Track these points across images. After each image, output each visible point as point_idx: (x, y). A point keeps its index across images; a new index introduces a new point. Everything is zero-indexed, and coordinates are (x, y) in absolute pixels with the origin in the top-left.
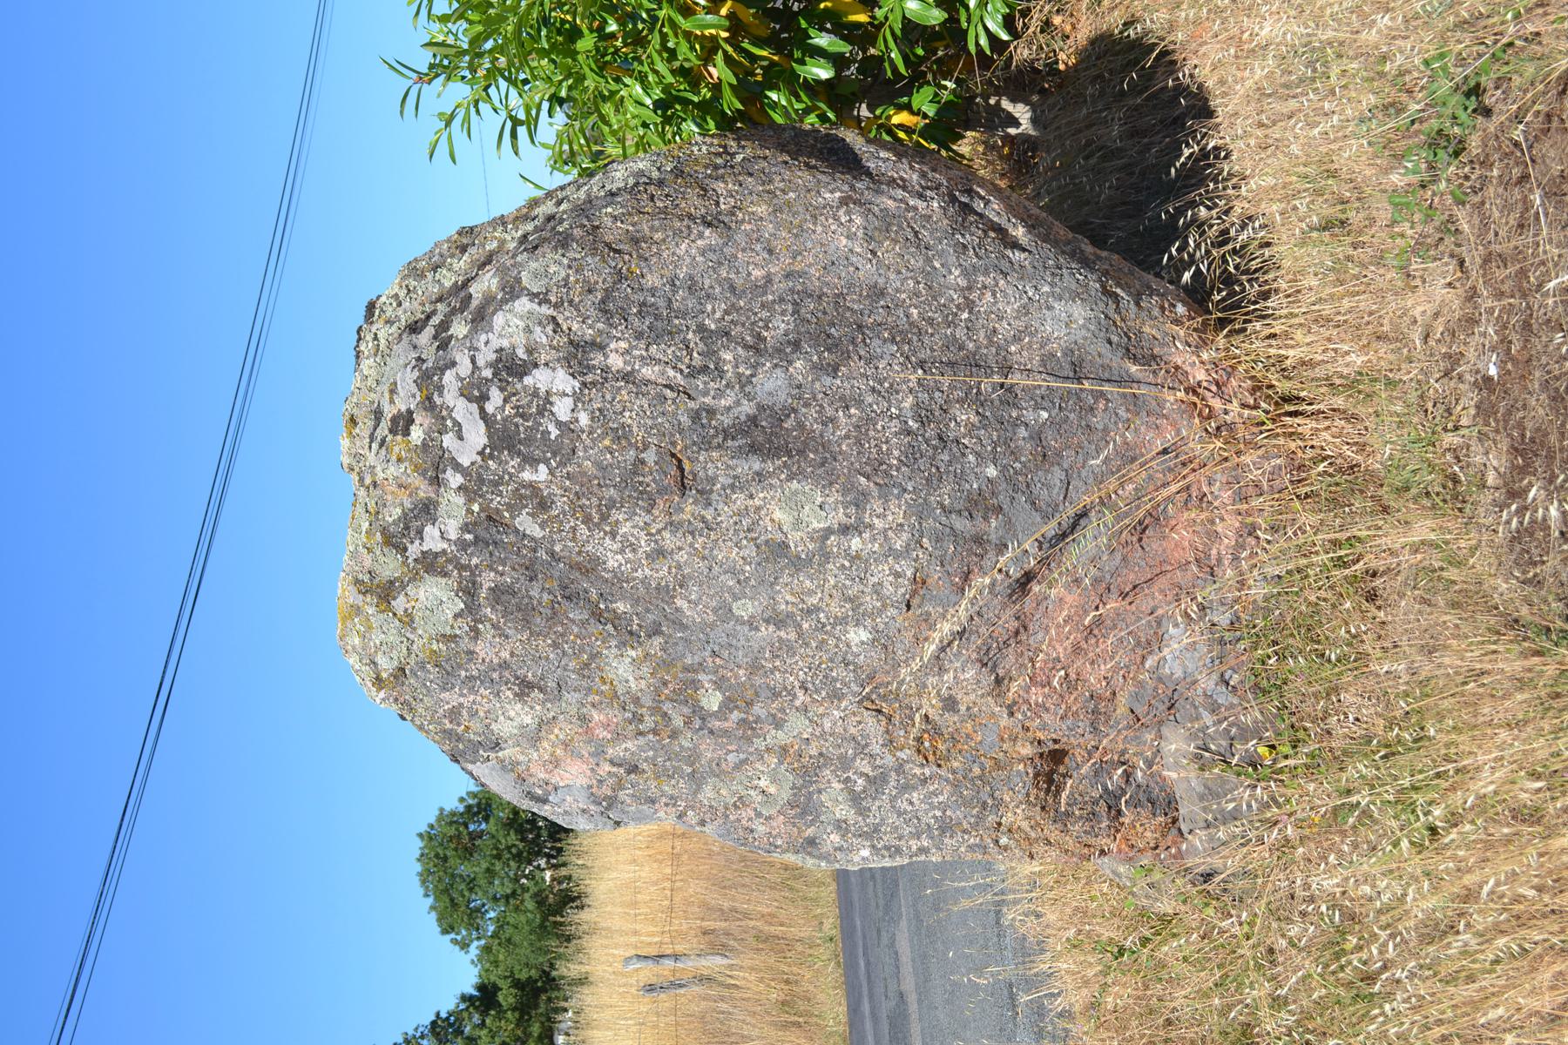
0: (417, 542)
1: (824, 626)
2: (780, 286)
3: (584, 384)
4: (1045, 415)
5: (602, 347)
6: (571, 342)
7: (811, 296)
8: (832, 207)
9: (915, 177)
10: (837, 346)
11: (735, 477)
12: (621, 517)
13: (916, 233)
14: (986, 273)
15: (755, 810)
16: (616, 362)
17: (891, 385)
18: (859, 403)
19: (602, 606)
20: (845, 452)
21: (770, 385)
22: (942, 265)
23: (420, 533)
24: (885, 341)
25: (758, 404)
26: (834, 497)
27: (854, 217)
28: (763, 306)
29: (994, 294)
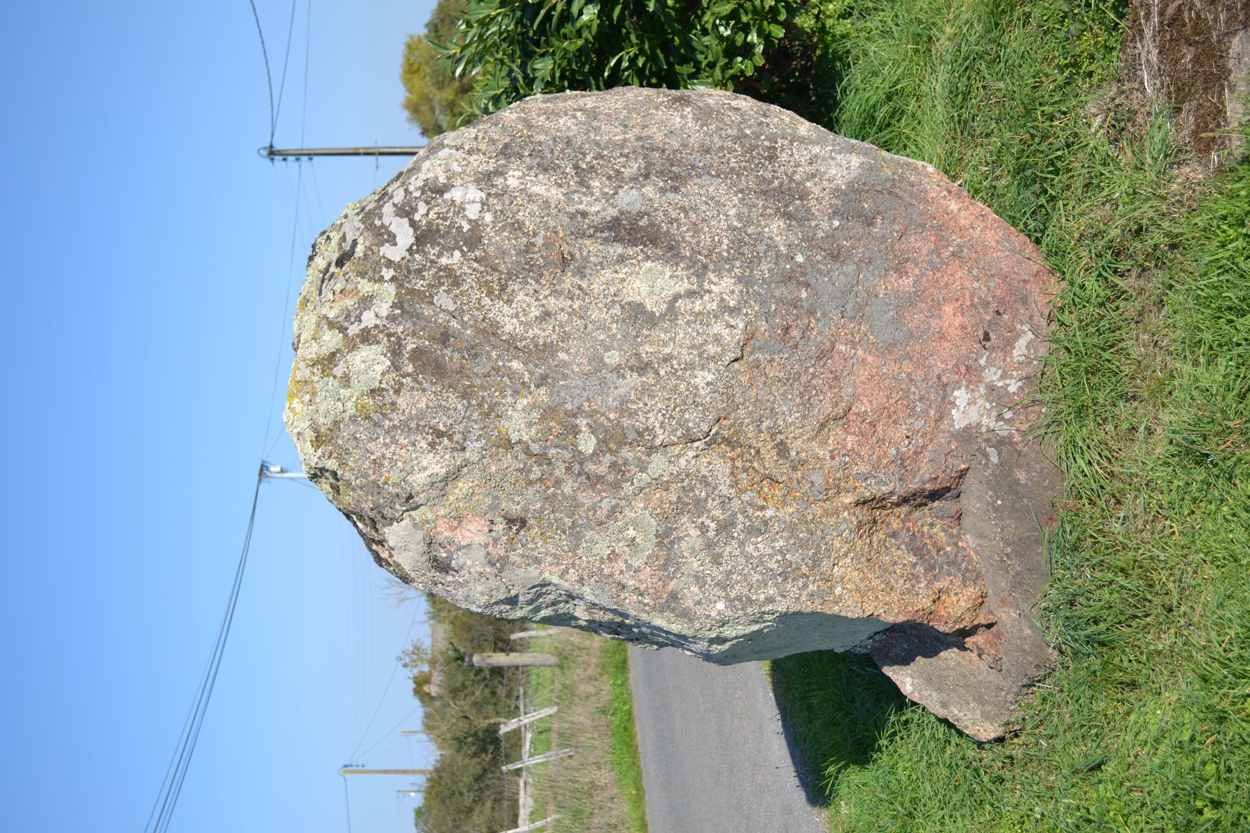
1: (676, 371)
3: (489, 195)
12: (516, 288)
15: (626, 561)
25: (620, 210)
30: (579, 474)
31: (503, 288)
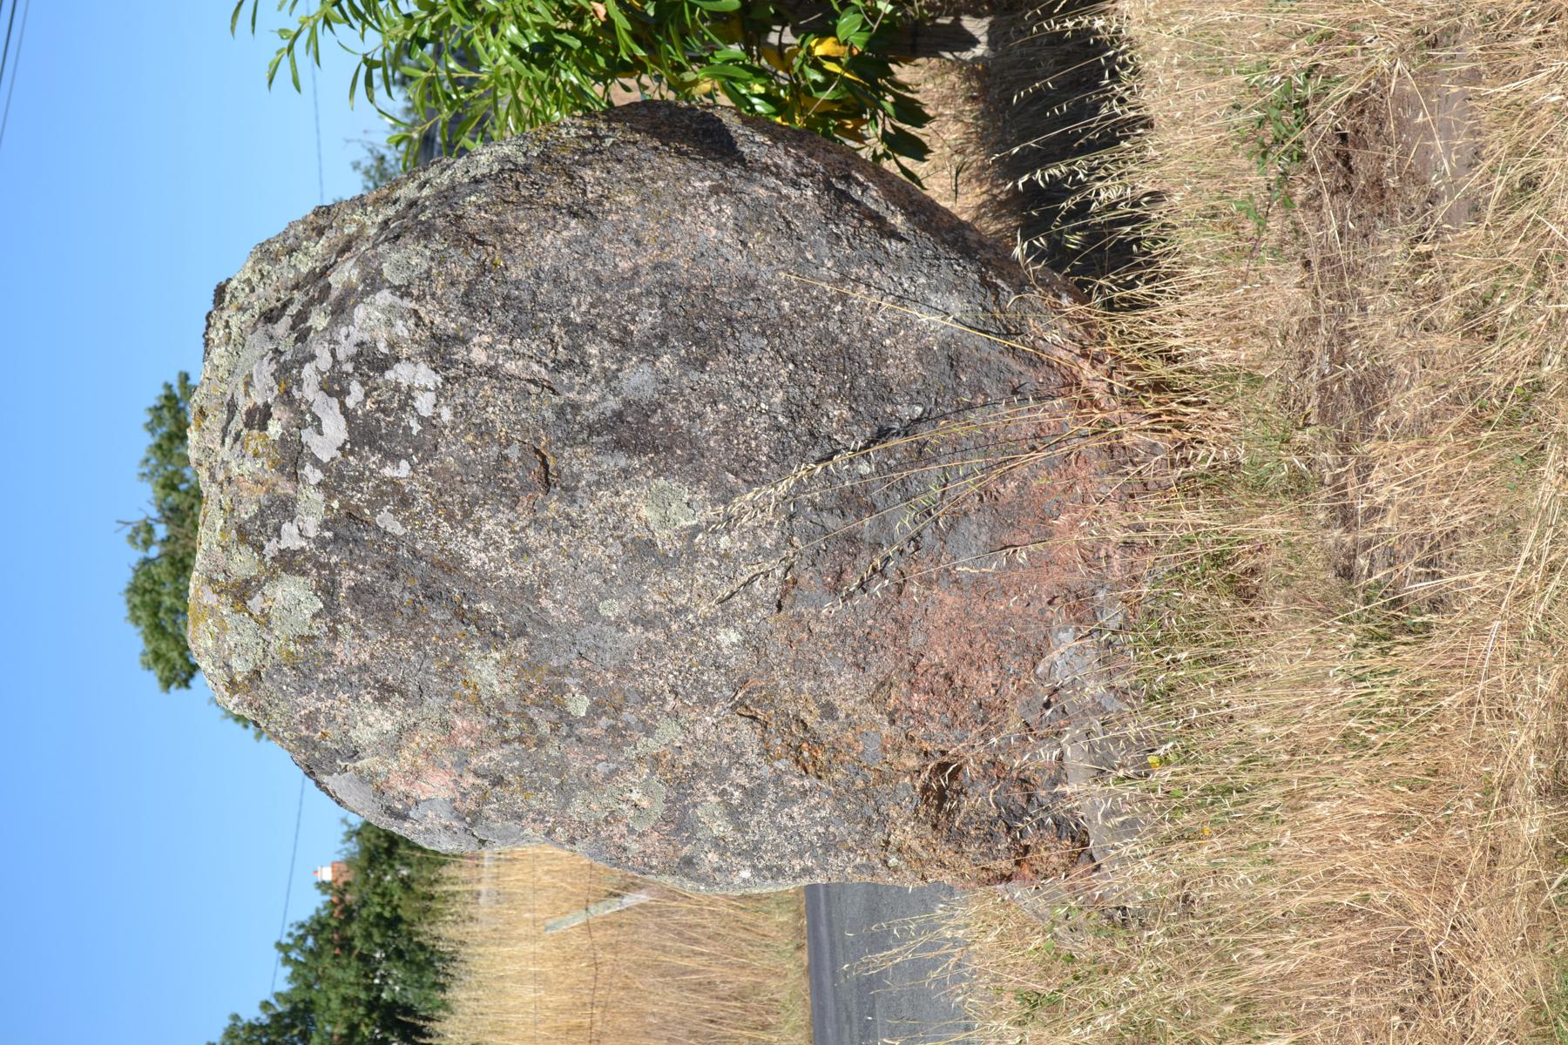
0: (275, 540)
2: (647, 279)
3: (447, 379)
5: (464, 342)
6: (433, 336)
7: (679, 288)
9: (790, 163)
11: (601, 474)
12: (484, 515)
13: (788, 223)
14: (860, 264)
16: (479, 356)
17: (761, 380)
18: (728, 398)
20: (713, 449)
21: (636, 380)
22: (815, 256)
23: (277, 530)
24: (755, 334)
25: (624, 400)
27: (724, 207)
28: (630, 299)
30: (568, 736)
31: (467, 515)
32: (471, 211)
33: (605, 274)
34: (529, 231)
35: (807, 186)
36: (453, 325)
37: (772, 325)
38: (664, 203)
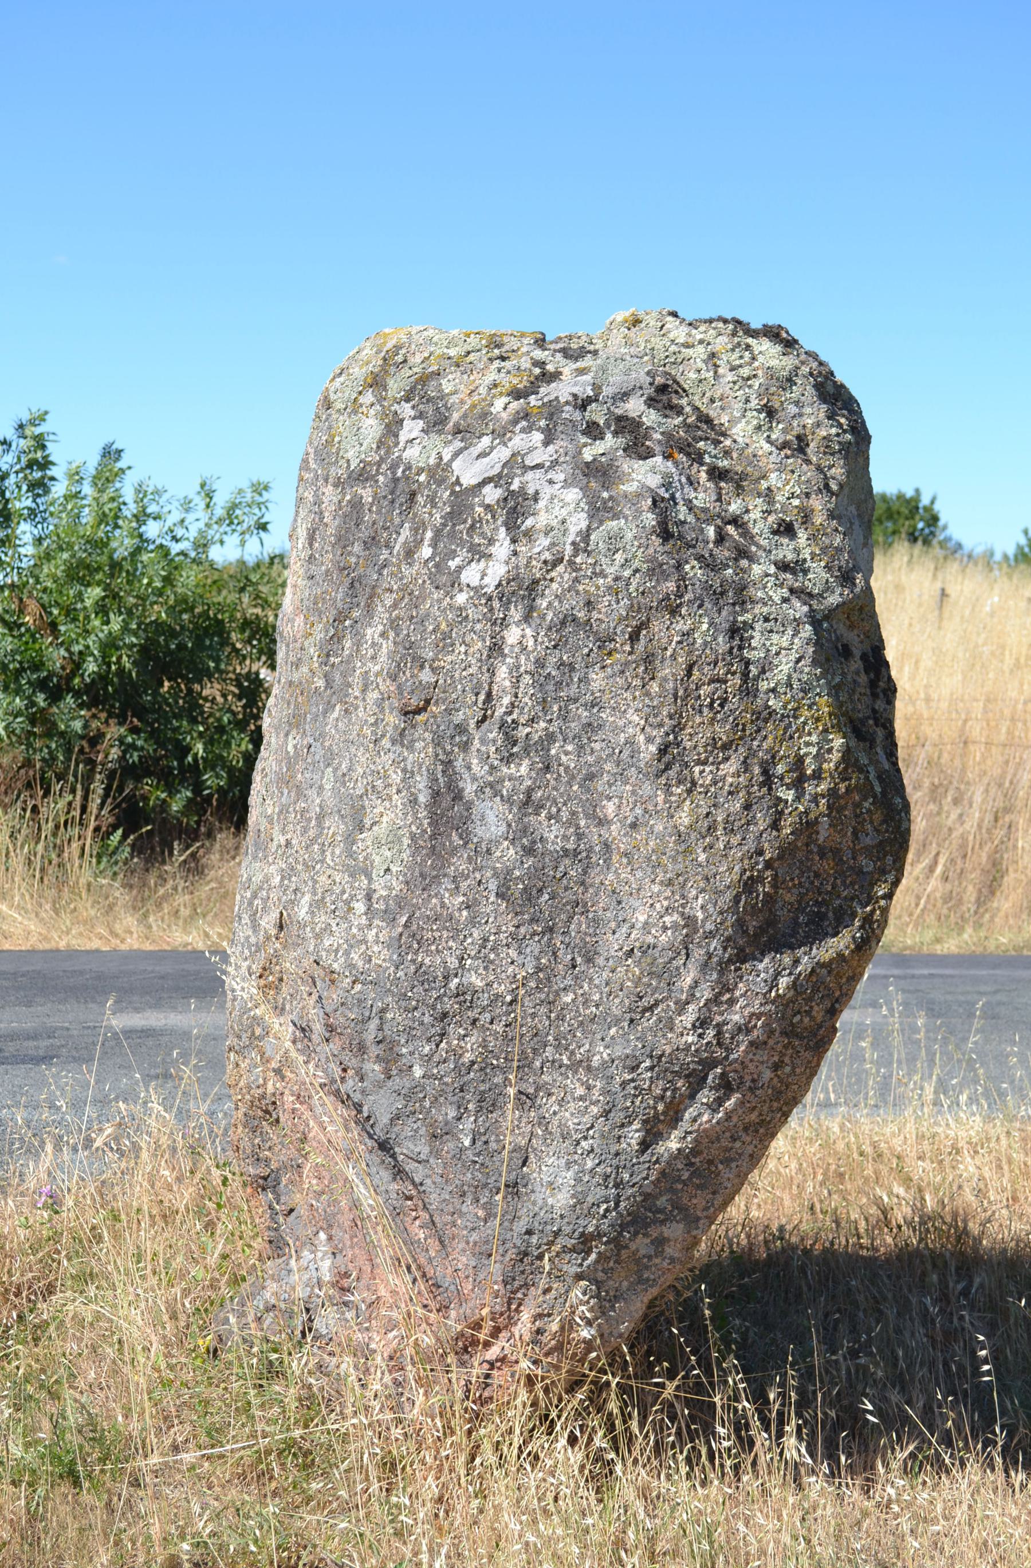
0: (412, 413)
2: (594, 835)
3: (490, 599)
4: (467, 1143)
5: (527, 618)
6: (536, 582)
7: (585, 872)
8: (683, 906)
9: (736, 1018)
10: (529, 900)
11: (412, 773)
13: (651, 1008)
14: (605, 1092)
16: (512, 635)
17: (492, 962)
18: (472, 922)
19: (347, 623)
20: (429, 901)
21: (491, 817)
22: (613, 1038)
23: (420, 416)
24: (538, 959)
26: (397, 886)
27: (669, 932)
28: (573, 813)
29: (581, 1098)
32: (681, 626)
33: (600, 785)
34: (648, 694)
35: (700, 1036)
36: (545, 604)
37: (548, 979)
38: (674, 859)
